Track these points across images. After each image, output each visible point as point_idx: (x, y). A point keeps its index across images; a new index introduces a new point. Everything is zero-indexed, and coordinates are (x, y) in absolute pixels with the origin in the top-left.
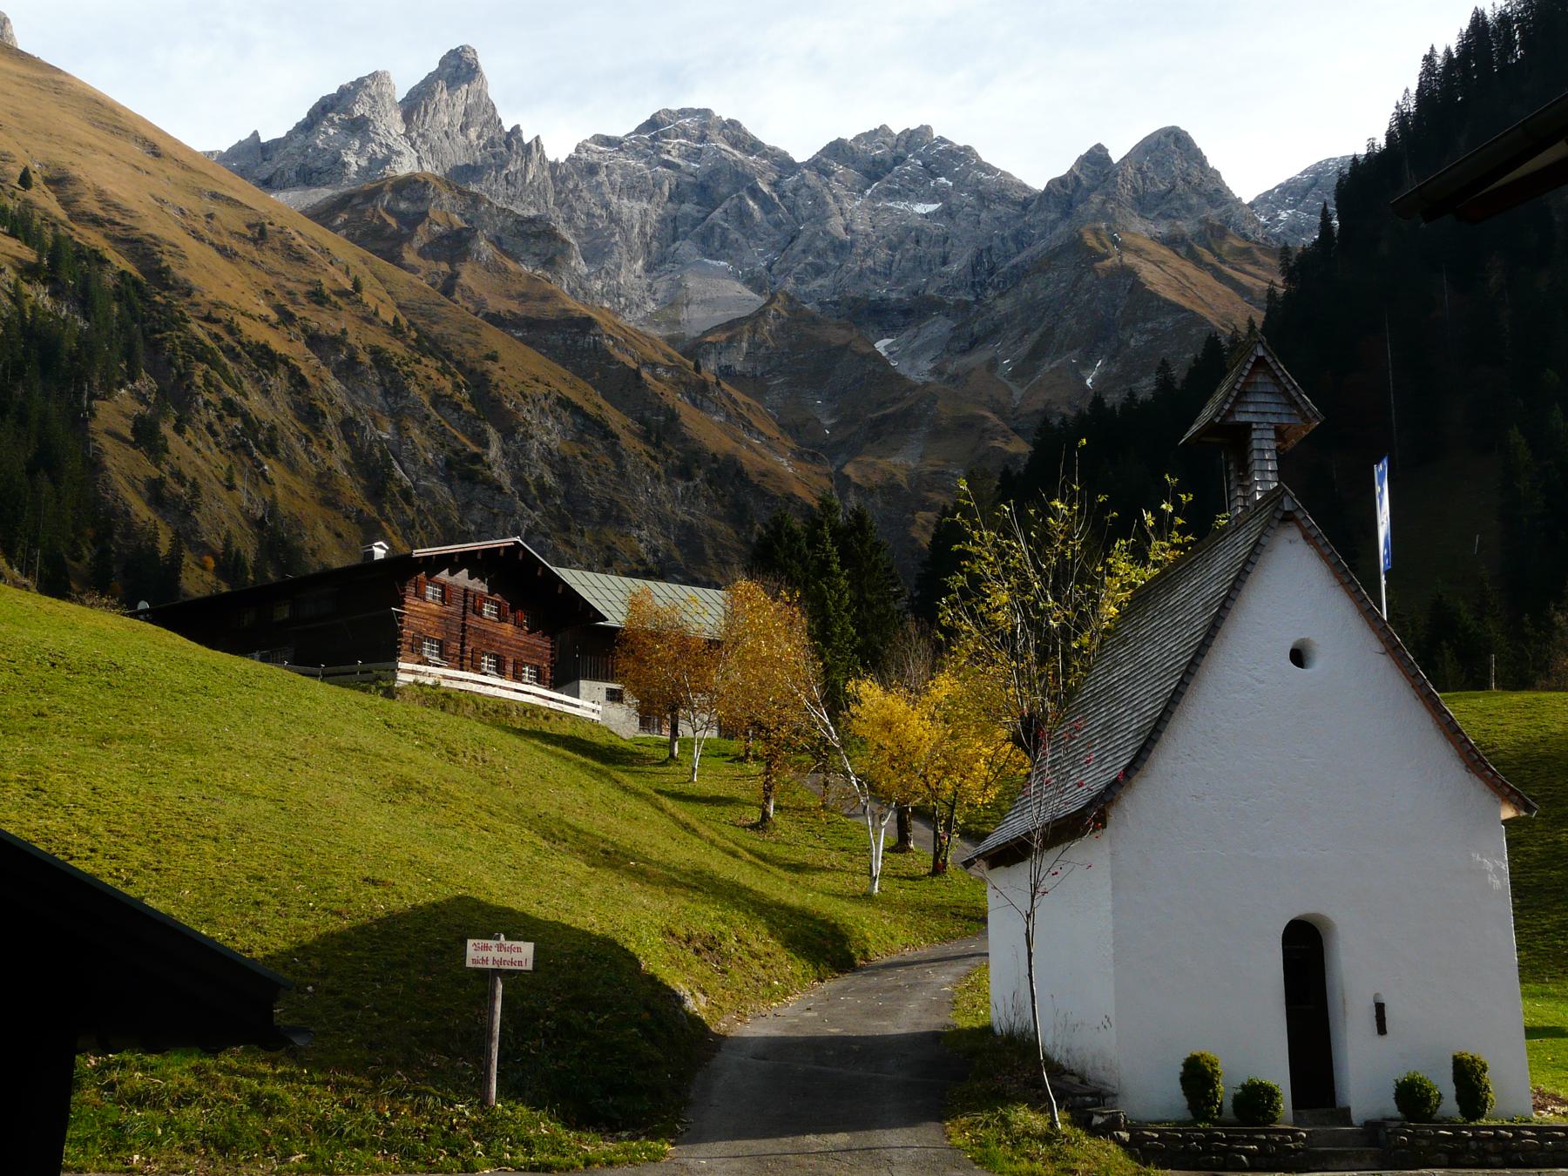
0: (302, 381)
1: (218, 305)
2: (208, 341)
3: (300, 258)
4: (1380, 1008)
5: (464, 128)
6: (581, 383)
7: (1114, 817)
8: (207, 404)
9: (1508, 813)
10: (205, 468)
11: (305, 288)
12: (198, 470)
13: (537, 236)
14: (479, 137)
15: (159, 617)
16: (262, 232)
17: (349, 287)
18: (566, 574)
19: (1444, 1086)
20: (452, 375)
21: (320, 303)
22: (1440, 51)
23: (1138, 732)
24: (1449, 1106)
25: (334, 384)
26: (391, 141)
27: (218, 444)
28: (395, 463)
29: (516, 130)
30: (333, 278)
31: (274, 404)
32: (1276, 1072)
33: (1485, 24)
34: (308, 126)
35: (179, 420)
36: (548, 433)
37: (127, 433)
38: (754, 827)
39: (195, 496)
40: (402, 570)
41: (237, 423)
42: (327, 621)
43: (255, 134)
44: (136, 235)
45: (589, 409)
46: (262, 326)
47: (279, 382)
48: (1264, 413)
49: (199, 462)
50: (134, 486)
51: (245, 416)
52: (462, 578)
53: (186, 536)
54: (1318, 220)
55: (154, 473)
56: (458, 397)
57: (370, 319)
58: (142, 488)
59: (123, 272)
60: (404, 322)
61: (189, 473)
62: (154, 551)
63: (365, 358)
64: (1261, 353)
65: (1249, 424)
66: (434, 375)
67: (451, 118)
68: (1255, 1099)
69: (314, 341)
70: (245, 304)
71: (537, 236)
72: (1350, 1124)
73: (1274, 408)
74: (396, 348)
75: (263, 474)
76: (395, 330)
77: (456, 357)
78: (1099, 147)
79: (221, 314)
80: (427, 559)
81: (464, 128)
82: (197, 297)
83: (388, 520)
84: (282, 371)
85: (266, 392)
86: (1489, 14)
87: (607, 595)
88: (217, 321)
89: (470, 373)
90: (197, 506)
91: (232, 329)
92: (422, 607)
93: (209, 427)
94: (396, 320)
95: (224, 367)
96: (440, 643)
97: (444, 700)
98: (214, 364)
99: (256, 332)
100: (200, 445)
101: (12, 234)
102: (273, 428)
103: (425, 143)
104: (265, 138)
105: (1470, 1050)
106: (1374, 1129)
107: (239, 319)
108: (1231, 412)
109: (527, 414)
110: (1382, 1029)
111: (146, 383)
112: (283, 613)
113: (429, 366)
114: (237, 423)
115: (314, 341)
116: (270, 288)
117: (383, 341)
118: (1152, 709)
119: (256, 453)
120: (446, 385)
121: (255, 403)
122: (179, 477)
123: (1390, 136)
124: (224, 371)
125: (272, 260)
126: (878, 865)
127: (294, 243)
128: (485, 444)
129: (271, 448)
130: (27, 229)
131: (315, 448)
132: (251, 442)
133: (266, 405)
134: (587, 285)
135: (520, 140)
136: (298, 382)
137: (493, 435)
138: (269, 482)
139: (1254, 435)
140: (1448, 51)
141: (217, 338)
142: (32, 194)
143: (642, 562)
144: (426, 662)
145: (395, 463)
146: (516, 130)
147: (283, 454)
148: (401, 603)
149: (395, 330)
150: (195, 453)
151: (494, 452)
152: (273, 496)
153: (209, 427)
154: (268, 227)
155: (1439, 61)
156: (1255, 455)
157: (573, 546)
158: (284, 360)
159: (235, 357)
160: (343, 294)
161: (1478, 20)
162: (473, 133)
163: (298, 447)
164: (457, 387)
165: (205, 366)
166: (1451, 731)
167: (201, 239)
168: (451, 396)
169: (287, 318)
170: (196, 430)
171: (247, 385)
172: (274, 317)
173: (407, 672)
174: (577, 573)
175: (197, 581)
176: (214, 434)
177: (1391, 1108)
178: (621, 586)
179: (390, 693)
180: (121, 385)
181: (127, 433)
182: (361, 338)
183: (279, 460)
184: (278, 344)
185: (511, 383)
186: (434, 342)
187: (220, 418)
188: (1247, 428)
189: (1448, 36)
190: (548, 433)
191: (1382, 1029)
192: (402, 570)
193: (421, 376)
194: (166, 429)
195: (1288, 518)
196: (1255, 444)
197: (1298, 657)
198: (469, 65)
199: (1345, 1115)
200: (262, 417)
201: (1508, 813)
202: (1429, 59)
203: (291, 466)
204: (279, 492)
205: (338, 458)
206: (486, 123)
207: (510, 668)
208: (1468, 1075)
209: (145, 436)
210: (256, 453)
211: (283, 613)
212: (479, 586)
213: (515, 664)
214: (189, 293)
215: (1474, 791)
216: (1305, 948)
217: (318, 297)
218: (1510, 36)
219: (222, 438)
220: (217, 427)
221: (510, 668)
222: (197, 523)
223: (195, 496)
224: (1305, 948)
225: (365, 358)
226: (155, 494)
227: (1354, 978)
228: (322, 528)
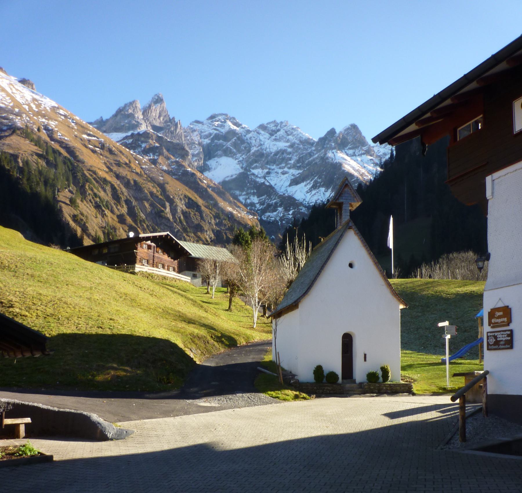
0: (115, 188)
2: (89, 176)
4: (365, 355)
5: (159, 117)
6: (191, 191)
7: (300, 305)
8: (89, 194)
9: (402, 307)
10: (89, 212)
12: (88, 213)
14: (163, 120)
15: (74, 251)
17: (128, 162)
18: (182, 243)
19: (380, 373)
20: (156, 188)
21: (119, 166)
24: (381, 379)
25: (124, 190)
26: (139, 121)
29: (174, 118)
30: (123, 159)
31: (108, 195)
32: (339, 371)
34: (116, 115)
36: (181, 206)
37: (68, 202)
38: (227, 310)
40: (137, 240)
41: (98, 200)
42: (117, 254)
43: (101, 117)
46: (104, 173)
47: (108, 188)
49: (88, 210)
50: (70, 216)
51: (100, 198)
52: (149, 242)
53: (85, 229)
54: (390, 152)
59: (66, 157)
61: (85, 213)
62: (76, 235)
63: (132, 182)
66: (151, 188)
67: (156, 114)
68: (333, 375)
69: (118, 177)
70: (99, 166)
75: (105, 214)
79: (92, 169)
80: (143, 238)
81: (159, 117)
83: (139, 228)
84: (109, 185)
85: (105, 191)
87: (194, 249)
91: (95, 173)
92: (142, 251)
93: (90, 200)
95: (94, 184)
96: (148, 260)
97: (149, 276)
98: (91, 183)
100: (88, 205)
101: (36, 145)
103: (148, 121)
104: (104, 119)
105: (384, 364)
107: (98, 171)
108: (338, 199)
109: (177, 201)
110: (365, 360)
111: (72, 187)
112: (105, 251)
116: (106, 162)
117: (137, 178)
118: (312, 278)
120: (155, 190)
121: (102, 194)
122: (82, 214)
125: (107, 154)
126: (256, 319)
128: (165, 208)
130: (39, 144)
131: (119, 207)
133: (106, 196)
134: (193, 163)
135: (174, 121)
136: (113, 188)
137: (167, 204)
139: (344, 205)
141: (91, 175)
142: (40, 134)
143: (207, 241)
144: (144, 265)
146: (174, 118)
147: (110, 209)
148: (136, 249)
150: (86, 208)
151: (168, 210)
152: (108, 220)
153: (90, 200)
157: (189, 236)
158: (110, 183)
160: (126, 164)
162: (161, 118)
163: (114, 207)
164: (158, 191)
166: (389, 285)
167: (86, 147)
169: (111, 170)
170: (87, 201)
172: (107, 170)
173: (138, 268)
175: (87, 242)
176: (92, 203)
179: (133, 273)
180: (66, 188)
181: (68, 202)
182: (131, 177)
183: (109, 210)
184: (109, 178)
185: (172, 191)
186: (151, 178)
187: (93, 198)
188: (342, 203)
190: (181, 206)
191: (365, 360)
192: (137, 240)
195: (350, 228)
197: (351, 265)
199: (354, 382)
200: (104, 198)
201: (402, 307)
203: (112, 212)
204: (110, 219)
205: (124, 210)
206: (165, 116)
207: (166, 267)
208: (385, 371)
211: (105, 251)
212: (153, 244)
213: (168, 266)
214: (83, 163)
215: (393, 300)
216: (348, 341)
217: (119, 164)
220: (92, 200)
221: (166, 267)
224: (348, 341)
225: (132, 182)
226: (74, 218)
227: (359, 349)
228: (121, 229)
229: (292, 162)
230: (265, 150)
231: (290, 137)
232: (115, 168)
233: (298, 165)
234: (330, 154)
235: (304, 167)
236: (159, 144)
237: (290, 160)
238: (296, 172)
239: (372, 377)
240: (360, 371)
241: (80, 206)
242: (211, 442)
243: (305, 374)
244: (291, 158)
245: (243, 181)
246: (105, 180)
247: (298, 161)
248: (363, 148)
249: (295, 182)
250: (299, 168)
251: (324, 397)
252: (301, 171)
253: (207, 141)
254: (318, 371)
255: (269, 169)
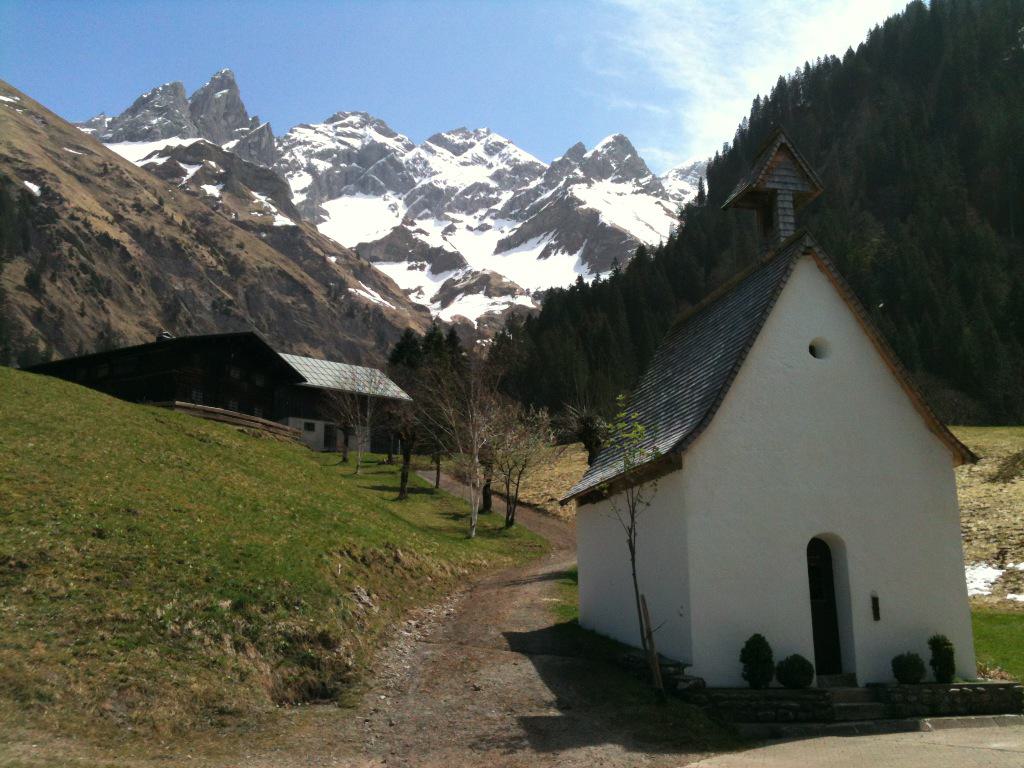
1: (79, 209)
2: (71, 230)
3: (128, 185)
4: (875, 601)
5: (225, 116)
11: (132, 202)
13: (268, 179)
16: (106, 169)
19: (926, 655)
20: (217, 255)
22: (762, 98)
23: (701, 403)
24: (930, 673)
27: (76, 290)
28: (182, 304)
32: (809, 653)
33: (785, 84)
35: (54, 275)
39: (61, 318)
41: (88, 277)
44: (31, 168)
45: (297, 277)
48: (786, 183)
51: (93, 274)
55: (36, 304)
56: (220, 268)
57: (170, 222)
58: (30, 313)
60: (188, 224)
64: (784, 140)
65: (775, 190)
69: (135, 232)
71: (268, 179)
72: (856, 685)
73: (793, 180)
74: (184, 239)
76: (183, 228)
77: (219, 245)
78: (580, 144)
79: (79, 214)
81: (225, 116)
82: (66, 204)
86: (787, 78)
88: (78, 219)
89: (228, 255)
90: (62, 324)
91: (87, 225)
93: (72, 280)
94: (184, 222)
99: (100, 226)
102: (110, 281)
106: (875, 690)
107: (91, 219)
110: (877, 616)
113: (204, 250)
114: (88, 277)
115: (135, 232)
119: (124, 238)
121: (99, 267)
122: (53, 308)
123: (735, 141)
124: (80, 248)
127: (124, 176)
129: (108, 293)
132: (98, 287)
138: (107, 312)
139: (780, 198)
140: (766, 98)
145: (182, 304)
149: (183, 228)
153: (72, 280)
154: (109, 167)
155: (761, 103)
156: (780, 211)
159: (88, 240)
161: (781, 81)
165: (70, 245)
168: (216, 267)
169: (118, 219)
171: (94, 256)
172: (111, 218)
174: (297, 358)
176: (74, 284)
177: (886, 674)
178: (330, 367)
182: (165, 232)
183: (113, 300)
184: (114, 233)
189: (766, 90)
191: (877, 616)
193: (198, 255)
194: (45, 280)
196: (780, 205)
198: (229, 80)
199: (851, 680)
202: (756, 101)
209: (33, 285)
210: (124, 238)
216: (822, 558)
217: (138, 208)
218: (797, 91)
219: (79, 286)
222: (62, 334)
223: (61, 318)
224: (822, 558)
226: (37, 317)
227: (859, 580)
229: (499, 207)
230: (445, 183)
231: (495, 159)
232: (135, 218)
233: (513, 213)
234: (579, 191)
235: (523, 218)
236: (584, 159)
237: (495, 203)
238: (508, 229)
239: (905, 666)
240: (869, 647)
241: (48, 289)
242: (827, 534)
243: (712, 658)
244: (497, 198)
245: (400, 246)
246: (105, 239)
247: (511, 205)
248: (641, 181)
249: (504, 246)
250: (515, 217)
251: (770, 744)
252: (519, 225)
253: (323, 166)
254: (756, 651)
255: (454, 221)
